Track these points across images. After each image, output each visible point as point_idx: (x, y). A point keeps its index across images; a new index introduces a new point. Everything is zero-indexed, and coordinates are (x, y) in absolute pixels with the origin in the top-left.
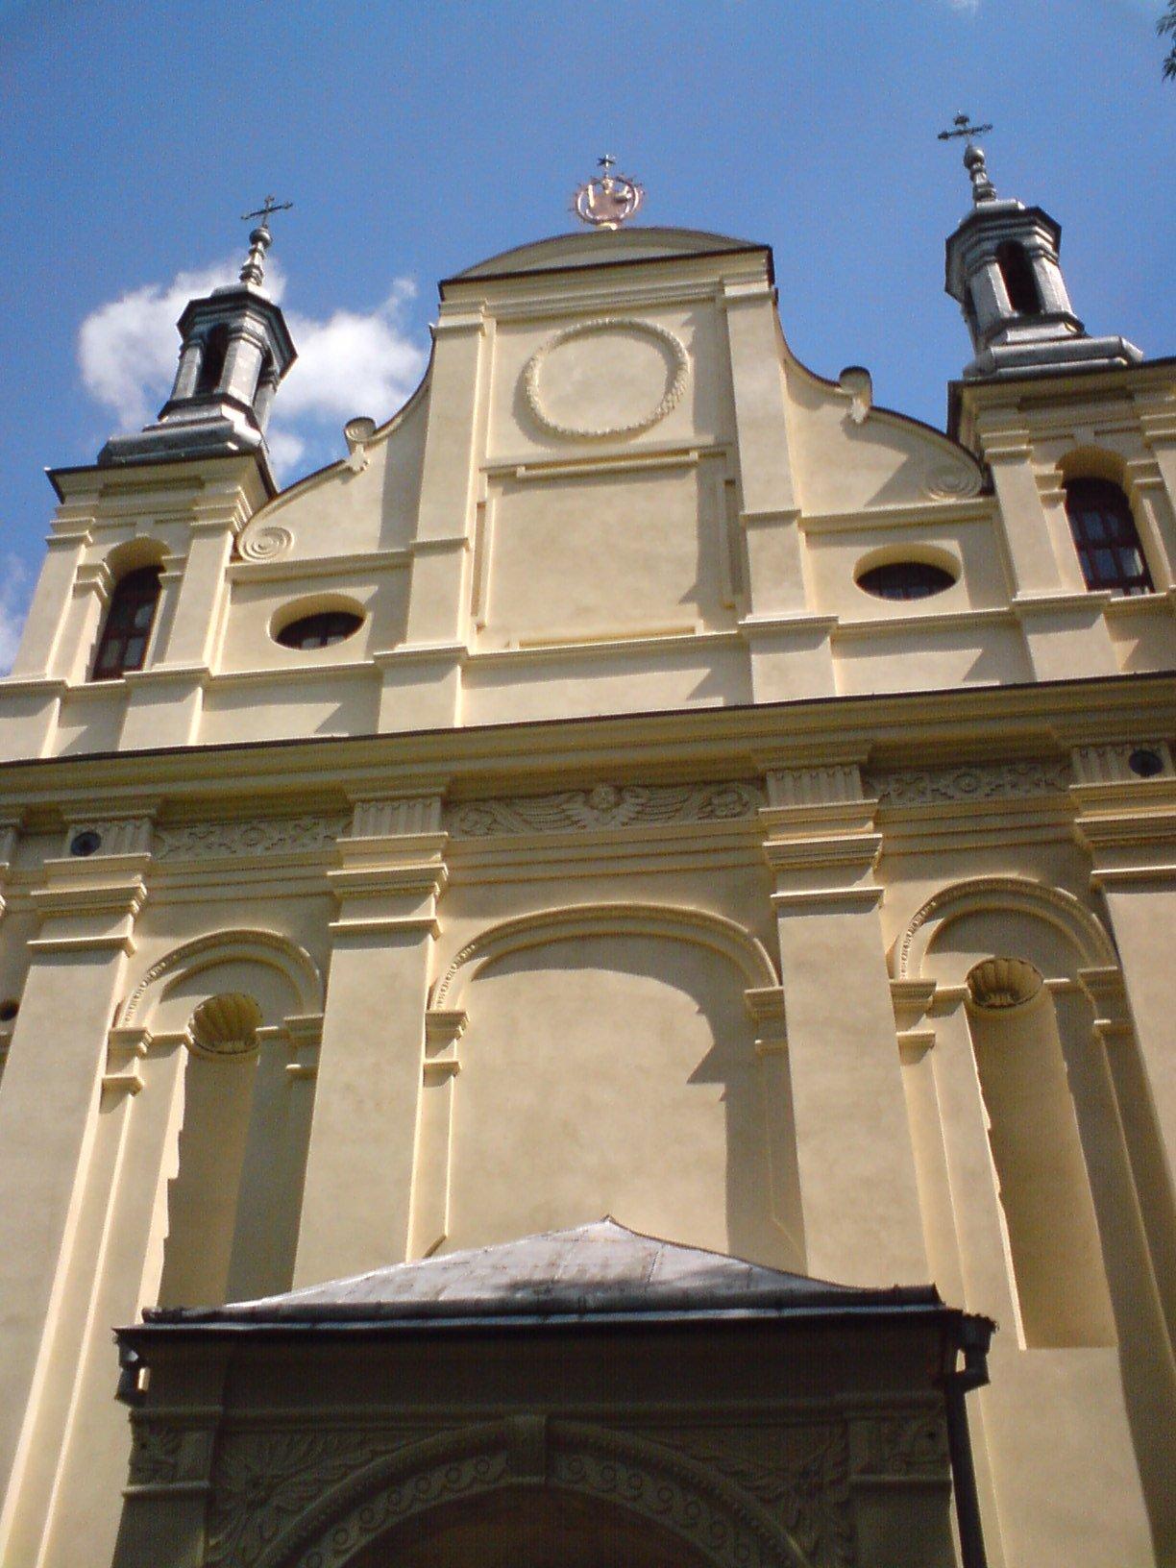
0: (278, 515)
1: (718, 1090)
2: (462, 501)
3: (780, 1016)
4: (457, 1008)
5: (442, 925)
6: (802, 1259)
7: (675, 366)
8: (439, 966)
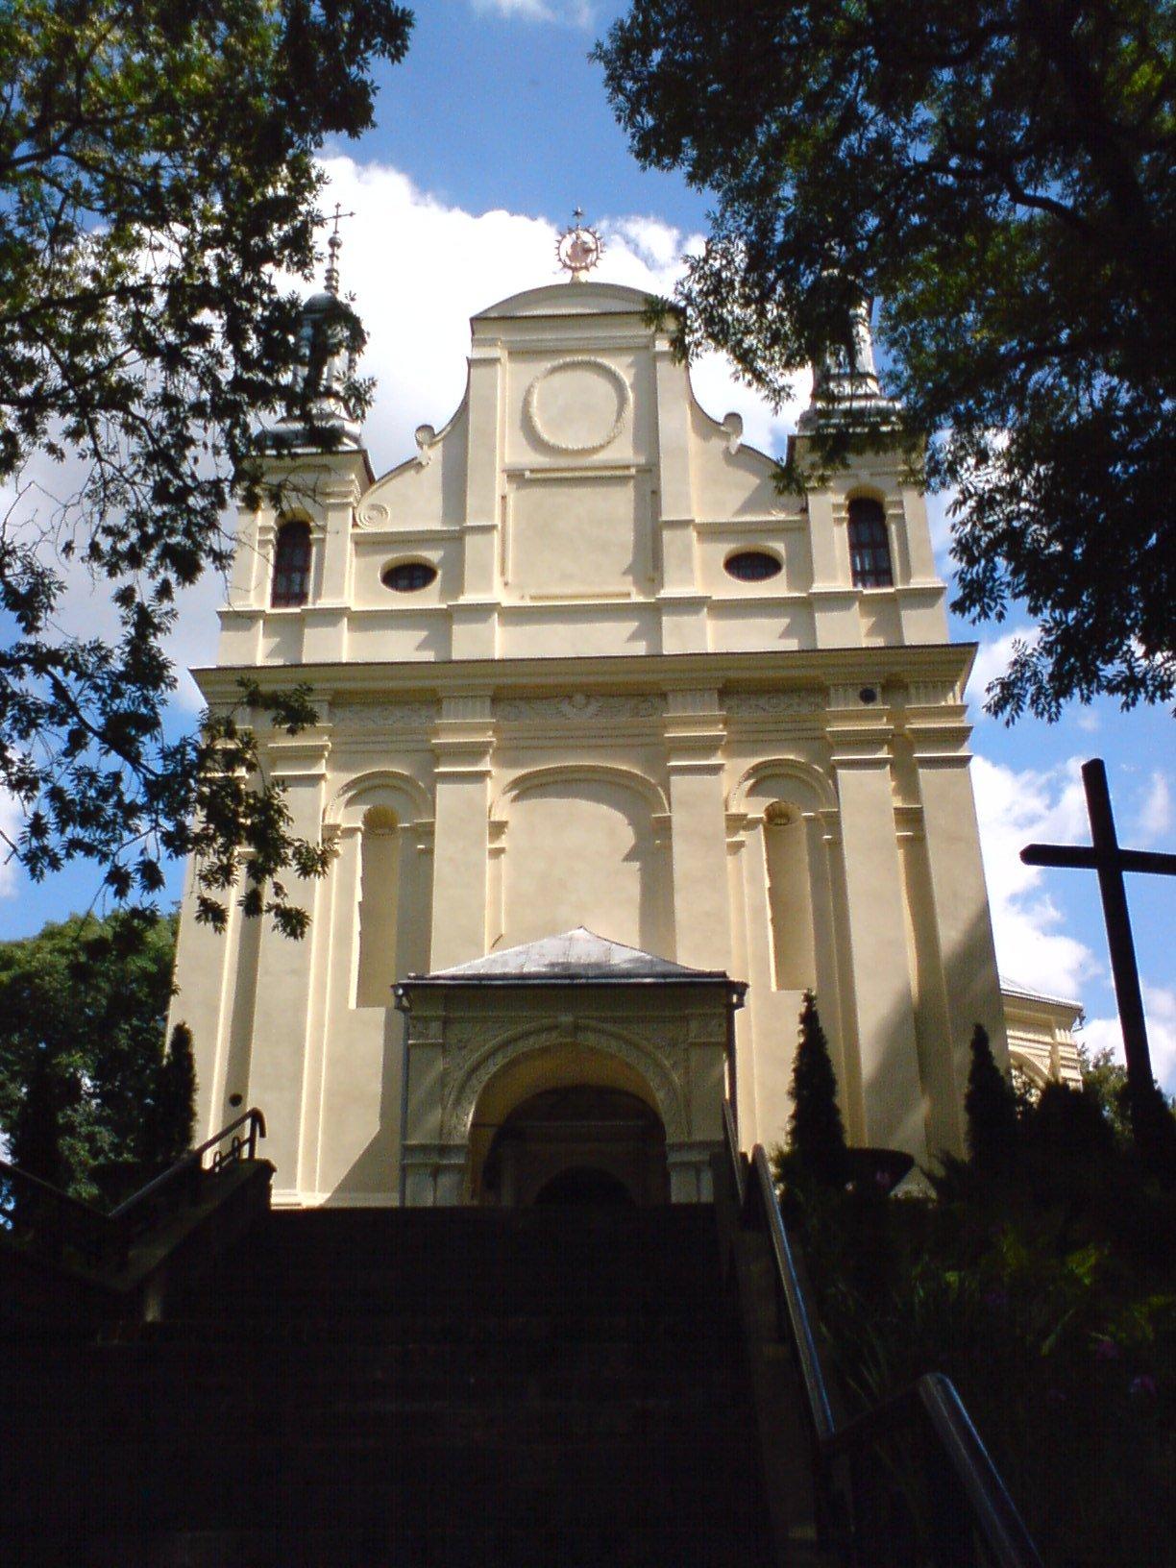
0: (375, 495)
1: (637, 865)
2: (492, 498)
3: (669, 829)
5: (329, 776)
6: (674, 952)
7: (622, 400)
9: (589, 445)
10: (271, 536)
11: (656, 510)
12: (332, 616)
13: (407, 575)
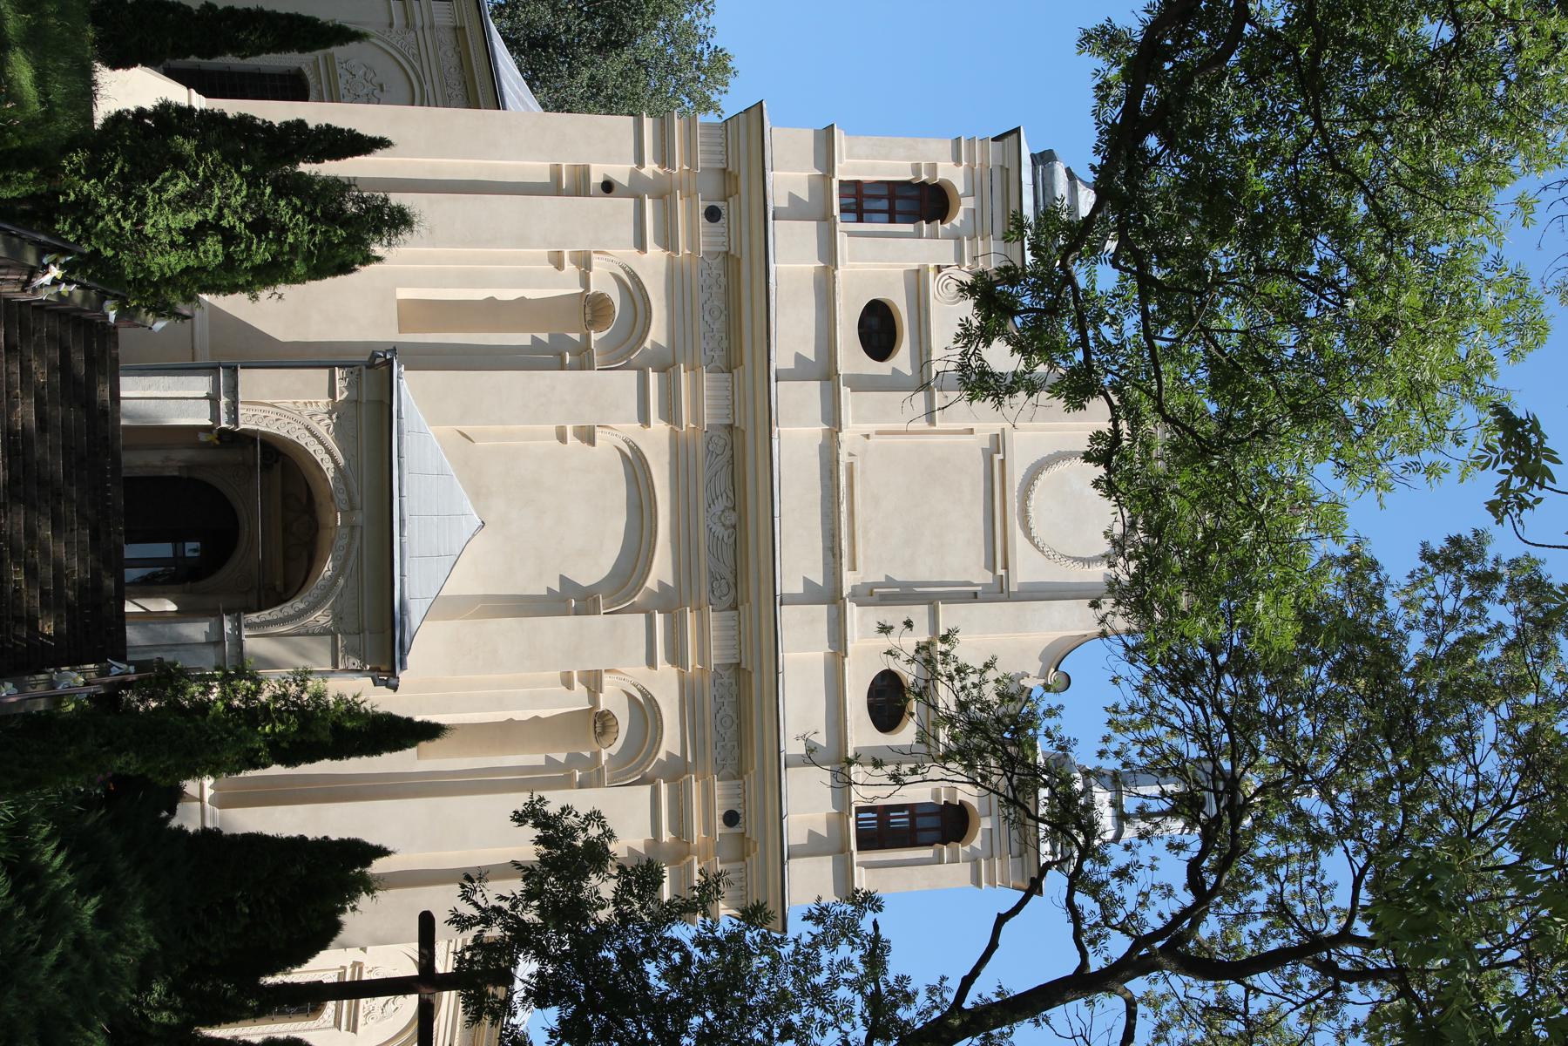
4: (597, 441)
8: (621, 429)
9: (1033, 523)
10: (924, 177)
11: (951, 598)
12: (829, 253)
13: (878, 330)
